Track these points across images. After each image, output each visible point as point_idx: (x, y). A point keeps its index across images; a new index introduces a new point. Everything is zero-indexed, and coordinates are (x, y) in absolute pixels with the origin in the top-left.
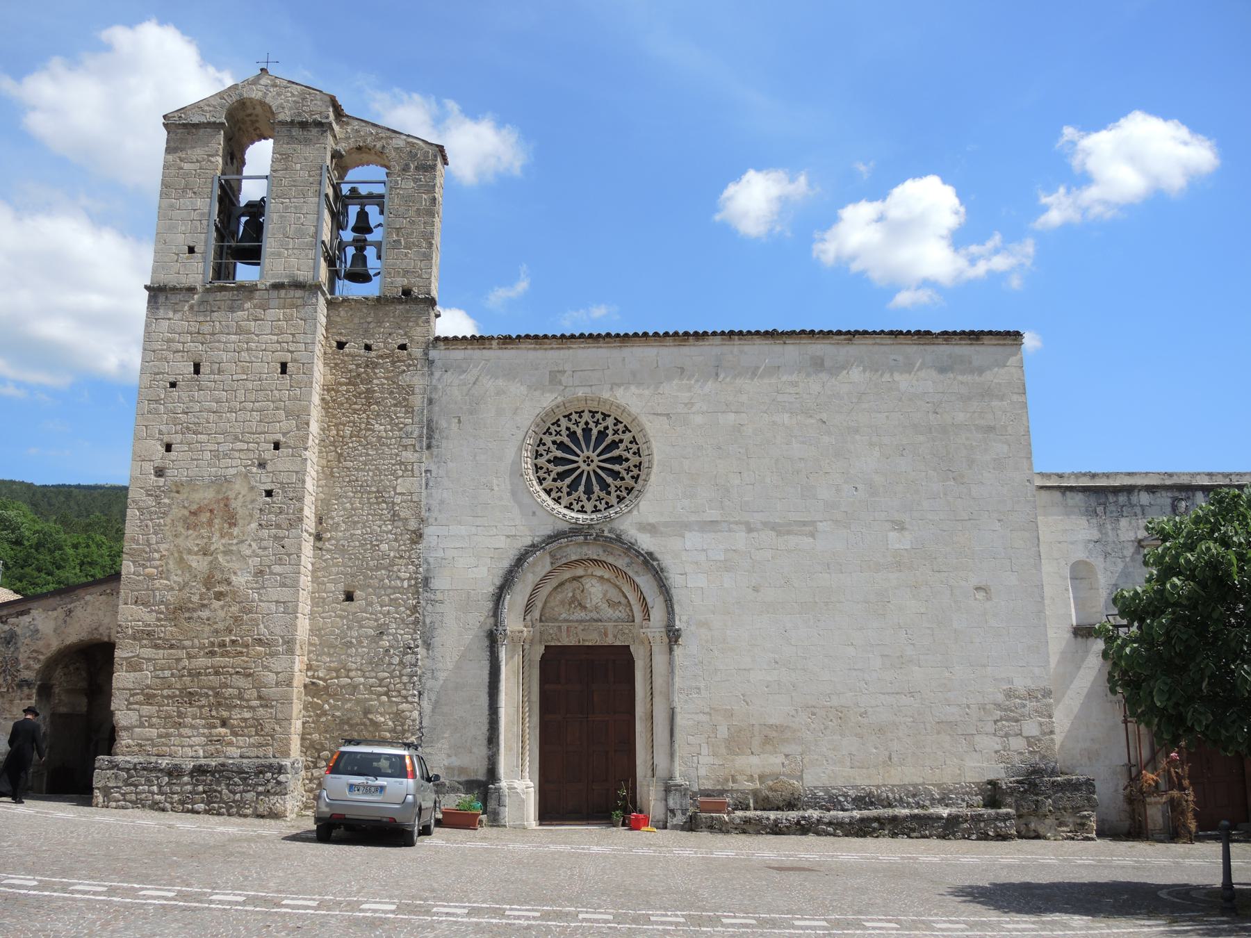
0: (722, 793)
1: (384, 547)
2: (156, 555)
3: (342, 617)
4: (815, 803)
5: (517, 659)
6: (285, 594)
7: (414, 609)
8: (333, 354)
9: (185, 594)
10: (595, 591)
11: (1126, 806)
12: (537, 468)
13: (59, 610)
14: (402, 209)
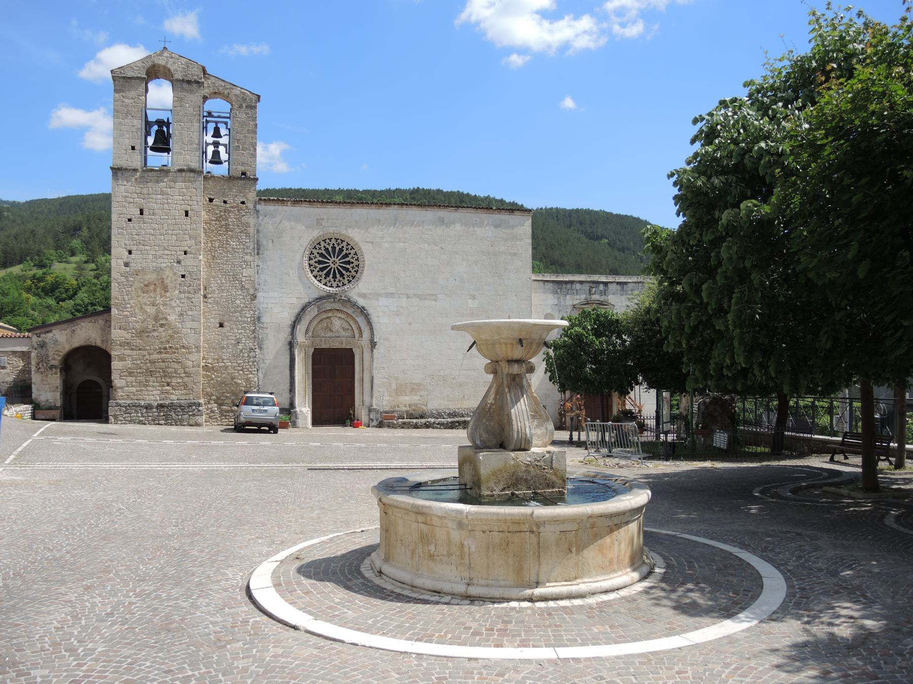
0: (392, 412)
1: (238, 302)
2: (129, 306)
3: (218, 335)
4: (432, 416)
5: (302, 354)
6: (195, 325)
7: (254, 331)
8: (207, 204)
9: (145, 325)
10: (337, 324)
11: (558, 417)
12: (310, 265)
14: (240, 129)
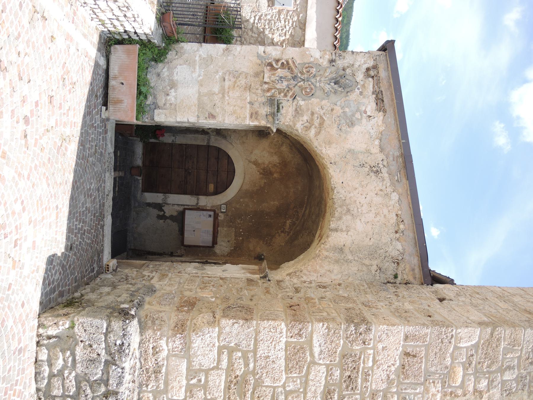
2: (483, 384)
13: (381, 156)
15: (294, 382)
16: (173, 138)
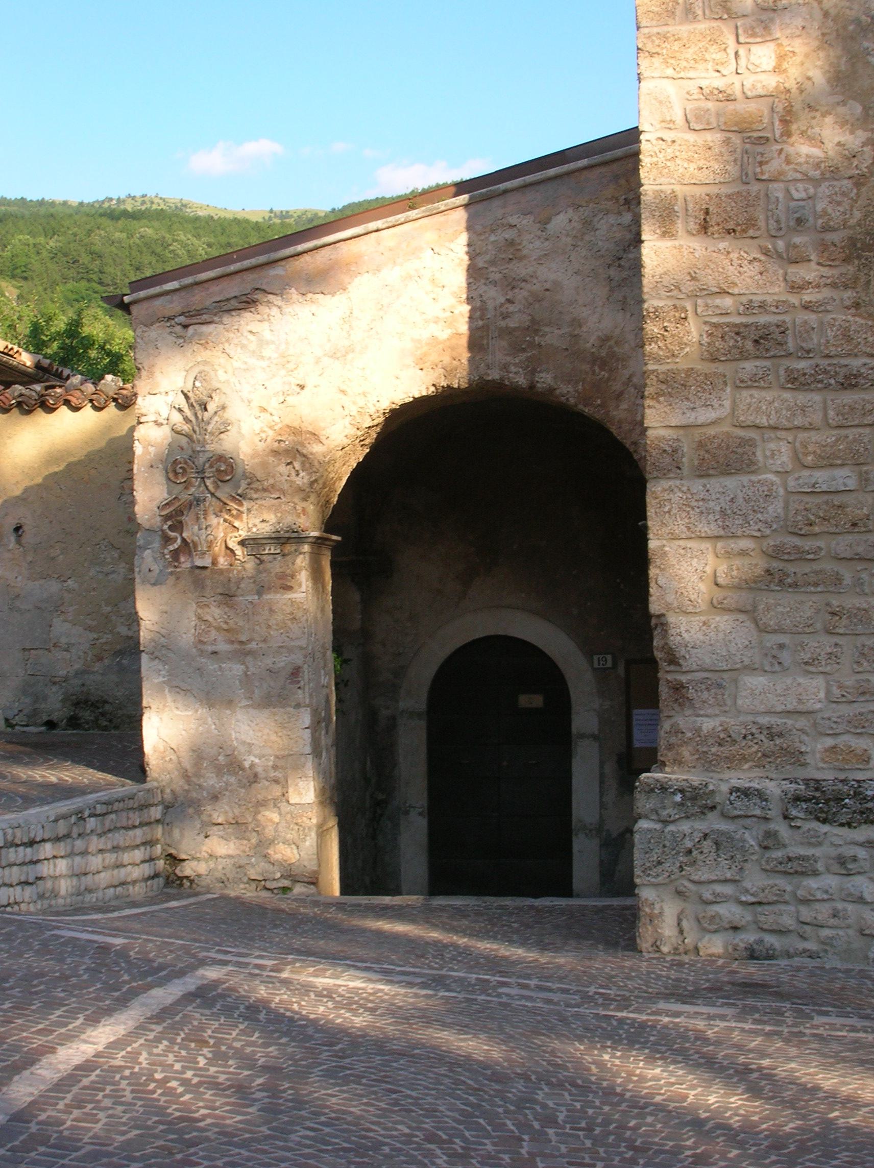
15: (773, 455)
16: (413, 813)
